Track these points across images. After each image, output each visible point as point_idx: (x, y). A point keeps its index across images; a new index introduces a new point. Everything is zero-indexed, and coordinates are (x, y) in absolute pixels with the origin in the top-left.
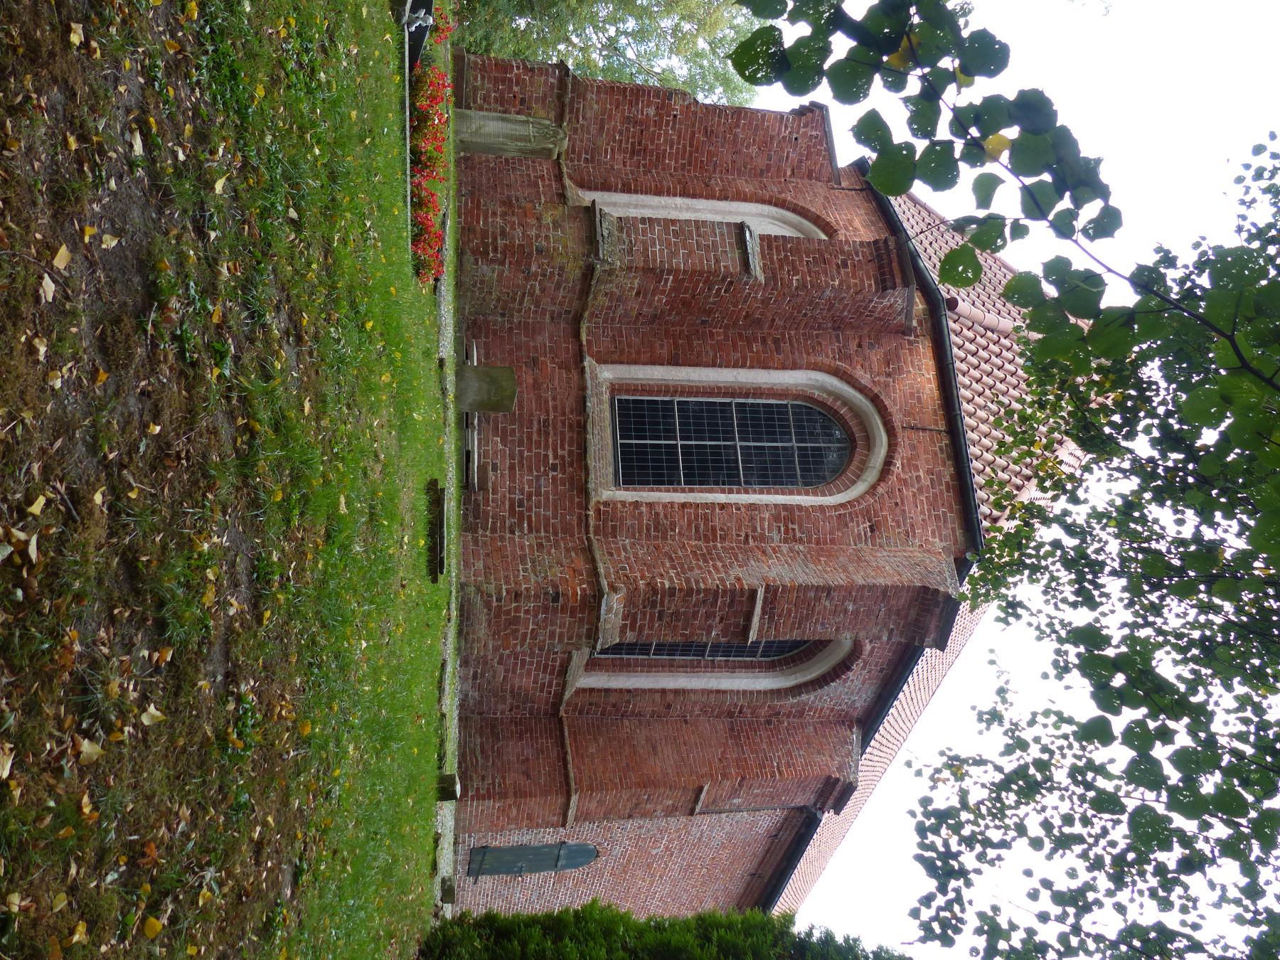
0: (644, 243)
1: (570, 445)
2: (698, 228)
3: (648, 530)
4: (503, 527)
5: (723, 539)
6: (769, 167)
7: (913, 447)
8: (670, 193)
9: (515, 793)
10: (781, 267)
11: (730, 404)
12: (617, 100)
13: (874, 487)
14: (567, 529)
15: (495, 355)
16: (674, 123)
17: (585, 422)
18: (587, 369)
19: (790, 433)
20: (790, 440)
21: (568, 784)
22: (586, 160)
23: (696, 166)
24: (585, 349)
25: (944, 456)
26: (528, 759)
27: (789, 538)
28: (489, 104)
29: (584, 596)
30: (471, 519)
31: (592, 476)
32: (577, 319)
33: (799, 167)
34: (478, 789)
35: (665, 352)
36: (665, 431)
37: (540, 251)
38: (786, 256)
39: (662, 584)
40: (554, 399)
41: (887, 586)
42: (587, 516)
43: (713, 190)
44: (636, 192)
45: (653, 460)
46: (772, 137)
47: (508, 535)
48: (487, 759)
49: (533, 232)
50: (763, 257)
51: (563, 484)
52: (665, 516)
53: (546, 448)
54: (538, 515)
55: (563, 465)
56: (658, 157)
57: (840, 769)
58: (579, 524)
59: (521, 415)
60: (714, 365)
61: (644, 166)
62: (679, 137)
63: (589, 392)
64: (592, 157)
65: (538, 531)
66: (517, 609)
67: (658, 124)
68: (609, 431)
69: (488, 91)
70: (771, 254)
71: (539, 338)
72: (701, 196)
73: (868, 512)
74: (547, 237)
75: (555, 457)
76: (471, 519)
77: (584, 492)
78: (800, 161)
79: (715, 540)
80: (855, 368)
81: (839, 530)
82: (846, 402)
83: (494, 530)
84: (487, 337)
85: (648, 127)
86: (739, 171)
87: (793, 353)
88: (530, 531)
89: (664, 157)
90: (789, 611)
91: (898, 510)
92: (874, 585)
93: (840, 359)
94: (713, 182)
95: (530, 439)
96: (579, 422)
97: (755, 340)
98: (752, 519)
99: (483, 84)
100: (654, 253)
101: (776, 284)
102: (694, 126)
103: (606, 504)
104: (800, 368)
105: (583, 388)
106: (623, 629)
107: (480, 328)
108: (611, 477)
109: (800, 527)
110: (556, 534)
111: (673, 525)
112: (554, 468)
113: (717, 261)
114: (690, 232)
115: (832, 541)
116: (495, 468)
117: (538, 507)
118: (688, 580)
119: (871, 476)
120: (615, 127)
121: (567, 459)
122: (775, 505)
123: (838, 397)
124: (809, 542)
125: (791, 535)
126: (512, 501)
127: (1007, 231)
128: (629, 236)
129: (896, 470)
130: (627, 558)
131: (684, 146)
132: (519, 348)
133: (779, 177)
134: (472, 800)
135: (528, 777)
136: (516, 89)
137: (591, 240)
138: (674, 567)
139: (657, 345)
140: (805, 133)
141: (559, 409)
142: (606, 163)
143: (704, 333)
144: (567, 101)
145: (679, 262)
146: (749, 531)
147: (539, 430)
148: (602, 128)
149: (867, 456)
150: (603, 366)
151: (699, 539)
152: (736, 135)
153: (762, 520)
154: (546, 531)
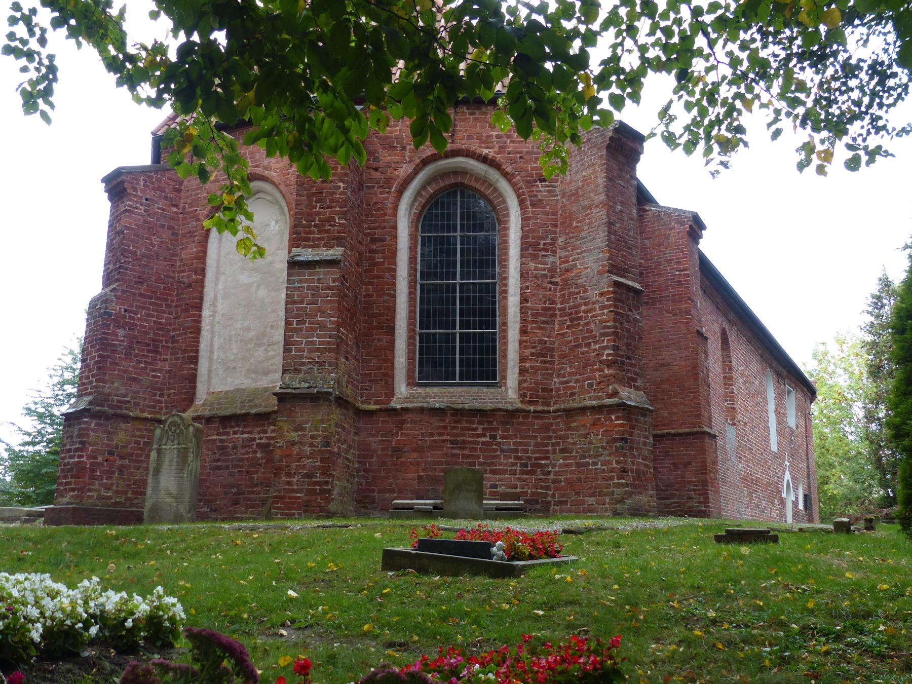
0: (311, 351)
1: (474, 423)
2: (294, 302)
3: (545, 362)
4: (545, 480)
5: (553, 302)
6: (170, 228)
7: (470, 137)
8: (198, 320)
9: (703, 474)
10: (328, 232)
11: (421, 285)
12: (111, 364)
13: (505, 175)
14: (546, 428)
15: (391, 485)
16: (131, 312)
17: (453, 409)
18: (404, 405)
19: (448, 237)
20: (455, 237)
21: (696, 433)
22: (161, 395)
23: (168, 295)
24: (384, 406)
25: (477, 112)
26: (674, 463)
27: (551, 248)
28: (112, 484)
29: (624, 418)
30: (538, 507)
31: (500, 406)
32: (359, 412)
33: (171, 199)
34: (699, 503)
35: (385, 338)
36: (447, 342)
37: (327, 444)
38: (315, 226)
39: (608, 355)
40: (432, 435)
41: (606, 177)
42: (535, 412)
43: (196, 281)
44: (197, 351)
45: (474, 353)
46: (145, 222)
47: (552, 476)
48: (673, 496)
49: (308, 449)
50: (317, 246)
51: (507, 430)
52: (534, 347)
53: (477, 443)
54: (534, 452)
55: (491, 429)
56: (160, 329)
57: (681, 223)
58: (541, 418)
59: (447, 463)
60: (394, 296)
61: (167, 342)
62: (143, 308)
63: (425, 405)
64: (159, 389)
65: (548, 452)
66: (632, 472)
67: (132, 327)
68: (450, 389)
69: (101, 485)
70: (314, 239)
71: (374, 446)
72: (201, 293)
73: (528, 181)
74: (312, 437)
75: (484, 436)
76: (538, 507)
77: (513, 414)
78: (166, 198)
79: (554, 309)
80: (398, 176)
81: (544, 208)
82: (423, 188)
83: (548, 488)
84: (373, 491)
85: (135, 337)
86: (173, 255)
87: (384, 228)
88: (547, 458)
89: (160, 323)
90: (623, 256)
91: (527, 157)
92: (605, 187)
93: (390, 188)
94: (185, 280)
95: (468, 456)
96: (452, 415)
97: (373, 259)
98: (536, 277)
99: (95, 490)
100: (321, 343)
101: (344, 238)
102: (134, 294)
103: (523, 396)
104: (396, 222)
105: (422, 410)
106: (637, 388)
107: (364, 497)
108: (492, 390)
109: (542, 238)
110: (550, 438)
111: (542, 342)
112: (493, 437)
113: (329, 288)
114: (298, 309)
115: (555, 214)
116: (495, 486)
117: (527, 451)
118: (603, 335)
119: (494, 175)
120: (134, 367)
121: (485, 426)
122: (522, 256)
123: (418, 194)
124: (555, 233)
125: (549, 247)
126: (522, 473)
127: (800, 118)
128: (304, 364)
129: (492, 154)
130: (577, 381)
131: (151, 304)
132: (384, 463)
133: (178, 220)
134: (709, 507)
135: (689, 463)
136: (100, 459)
137: (315, 398)
138: (588, 345)
139: (378, 344)
140: (142, 191)
141: (441, 431)
142: (164, 378)
143: (365, 302)
144: (111, 411)
145: (330, 321)
146: (546, 280)
147: (461, 448)
148: (135, 380)
149: (472, 175)
150: (396, 391)
151: (554, 321)
152: (143, 256)
153: (536, 269)
154: (547, 445)
